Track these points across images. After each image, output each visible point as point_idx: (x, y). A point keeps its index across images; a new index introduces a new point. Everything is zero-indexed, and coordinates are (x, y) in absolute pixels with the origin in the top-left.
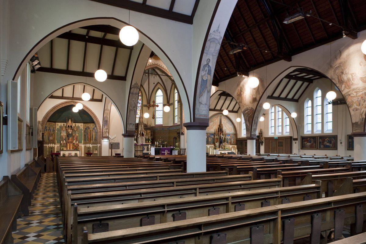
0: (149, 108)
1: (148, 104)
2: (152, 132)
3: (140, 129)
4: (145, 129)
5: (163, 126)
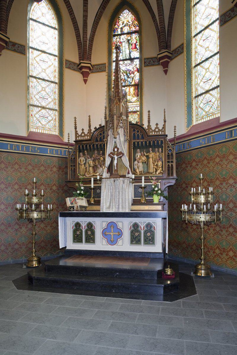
0: (85, 75)
1: (161, 48)
2: (169, 156)
3: (109, 149)
4: (134, 147)
5: (222, 120)
